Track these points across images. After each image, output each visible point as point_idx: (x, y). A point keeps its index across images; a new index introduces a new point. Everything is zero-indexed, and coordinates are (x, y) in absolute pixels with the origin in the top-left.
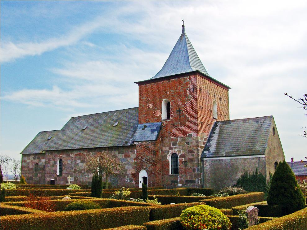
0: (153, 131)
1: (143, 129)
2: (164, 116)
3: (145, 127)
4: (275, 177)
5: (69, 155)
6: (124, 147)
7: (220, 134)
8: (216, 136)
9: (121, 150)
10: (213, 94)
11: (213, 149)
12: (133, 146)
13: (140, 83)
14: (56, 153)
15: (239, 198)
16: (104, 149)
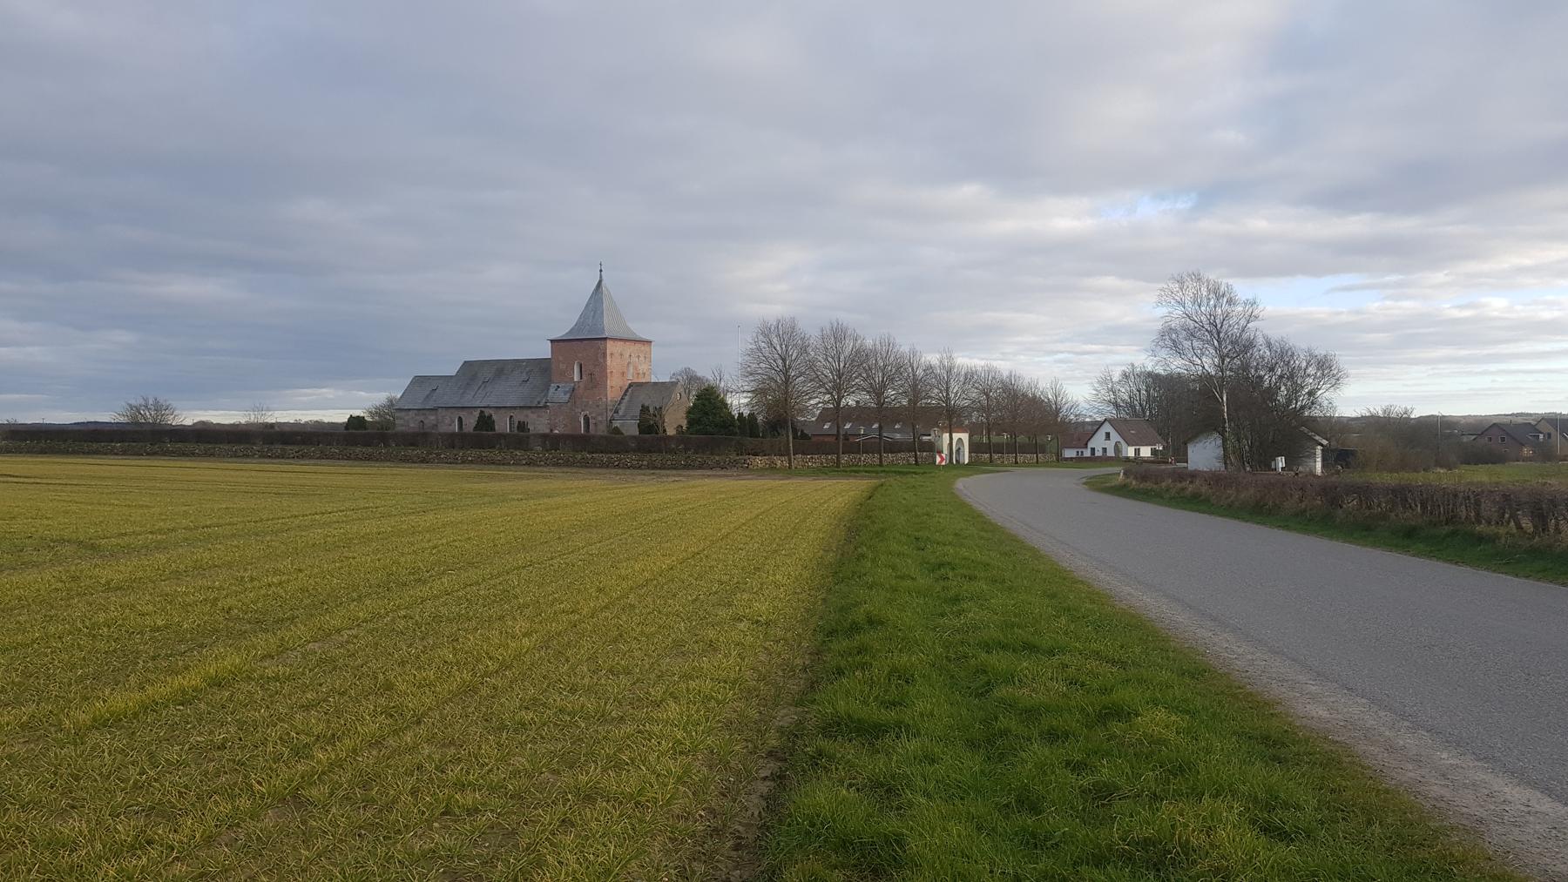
0: (565, 393)
1: (556, 390)
2: (576, 378)
3: (558, 387)
4: (1279, 524)
5: (472, 413)
6: (536, 407)
7: (631, 397)
8: (627, 398)
9: (533, 410)
10: (628, 354)
11: (621, 413)
12: (545, 407)
13: (552, 341)
14: (453, 410)
15: (899, 368)
16: (515, 408)
